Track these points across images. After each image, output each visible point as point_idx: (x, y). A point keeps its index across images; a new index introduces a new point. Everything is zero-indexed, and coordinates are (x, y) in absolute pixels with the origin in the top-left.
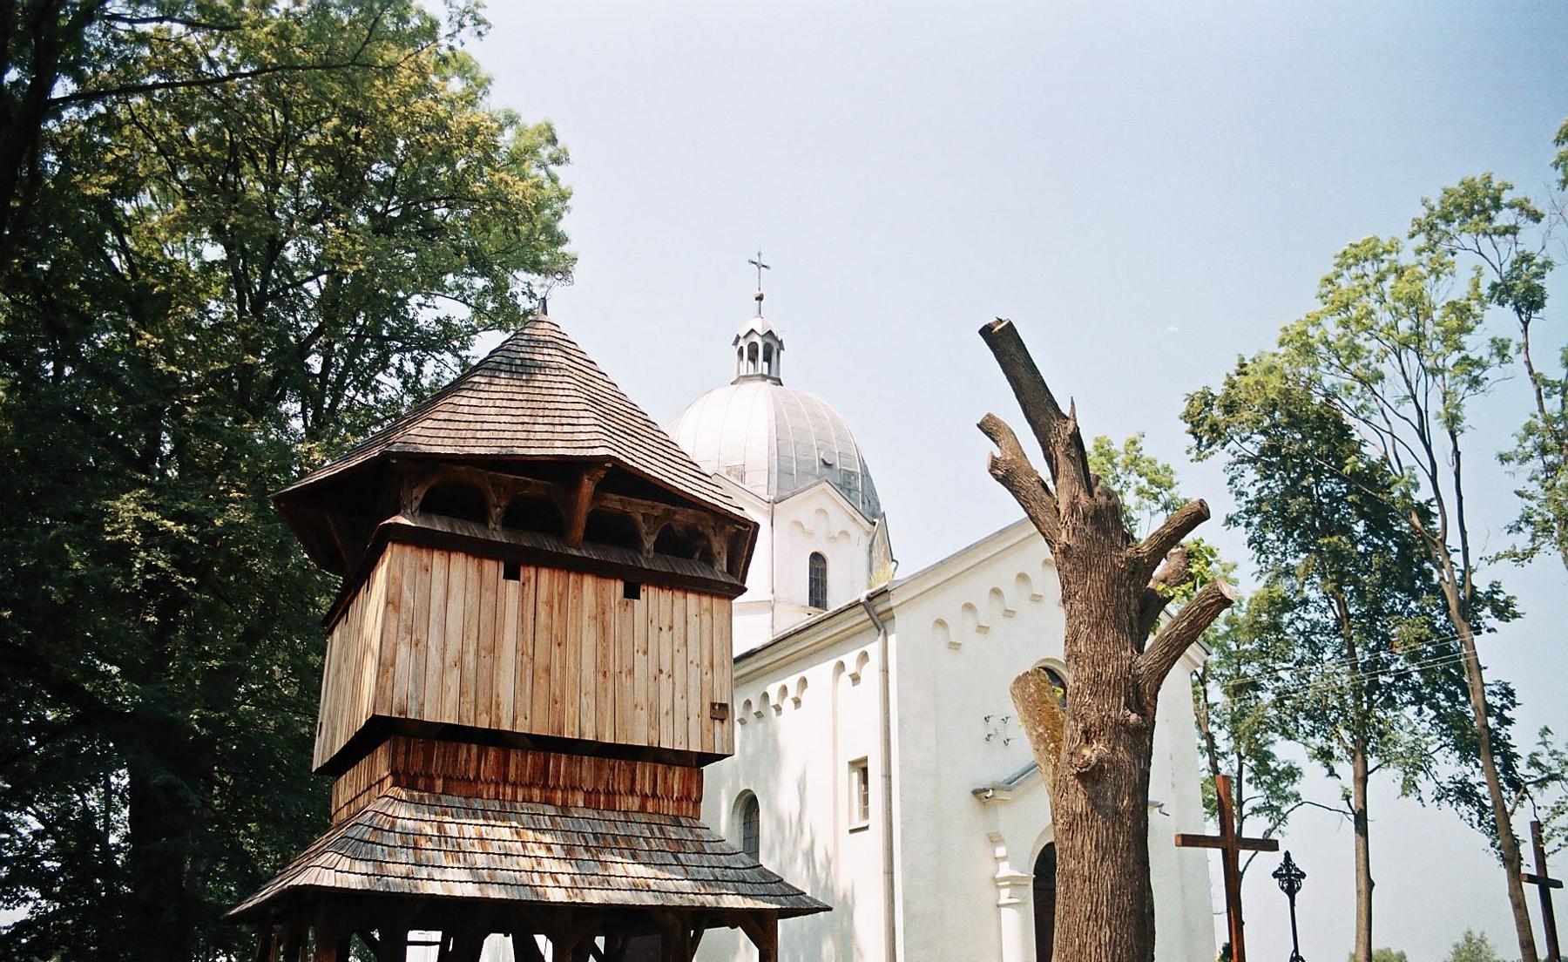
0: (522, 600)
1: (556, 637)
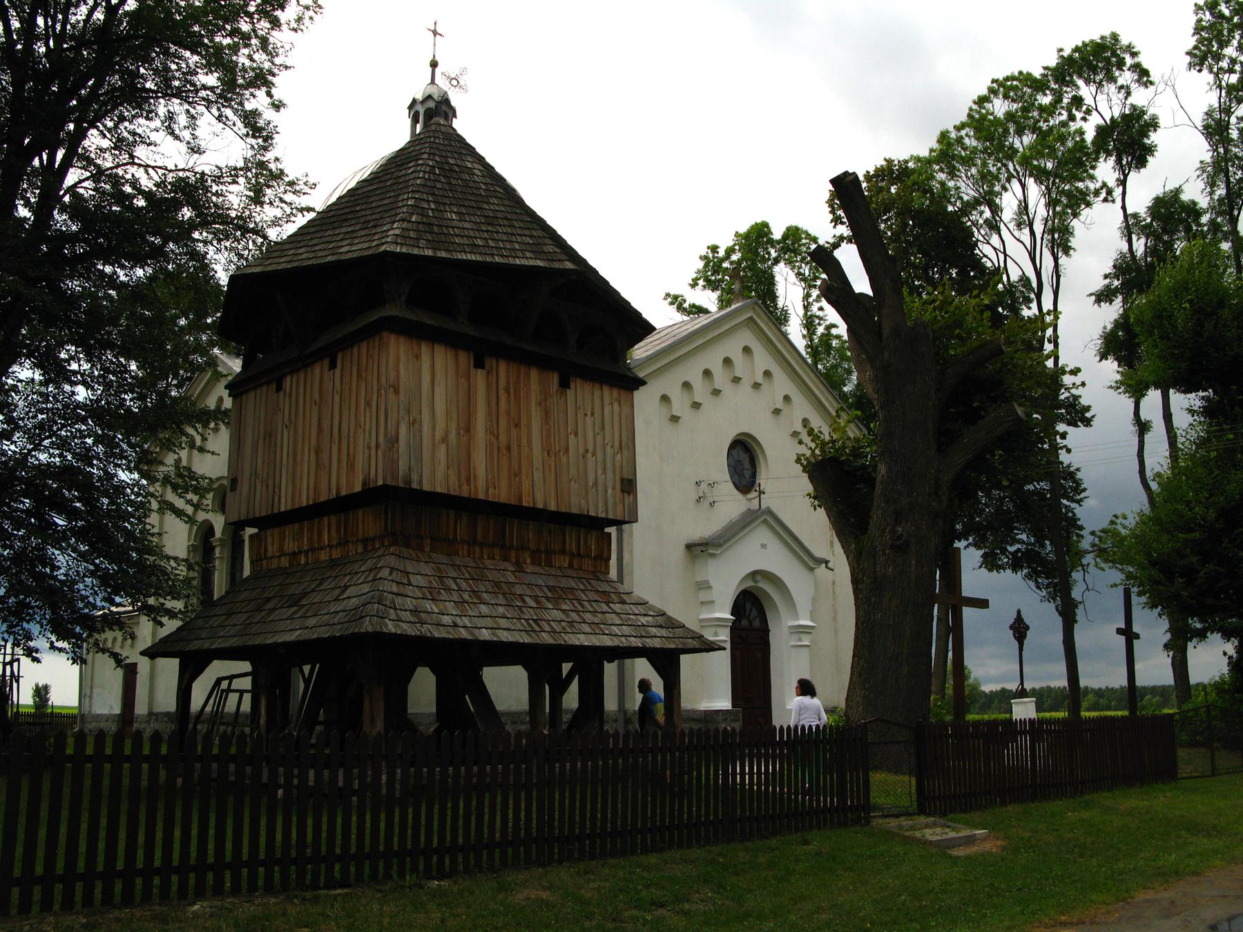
0: (488, 386)
1: (514, 419)
